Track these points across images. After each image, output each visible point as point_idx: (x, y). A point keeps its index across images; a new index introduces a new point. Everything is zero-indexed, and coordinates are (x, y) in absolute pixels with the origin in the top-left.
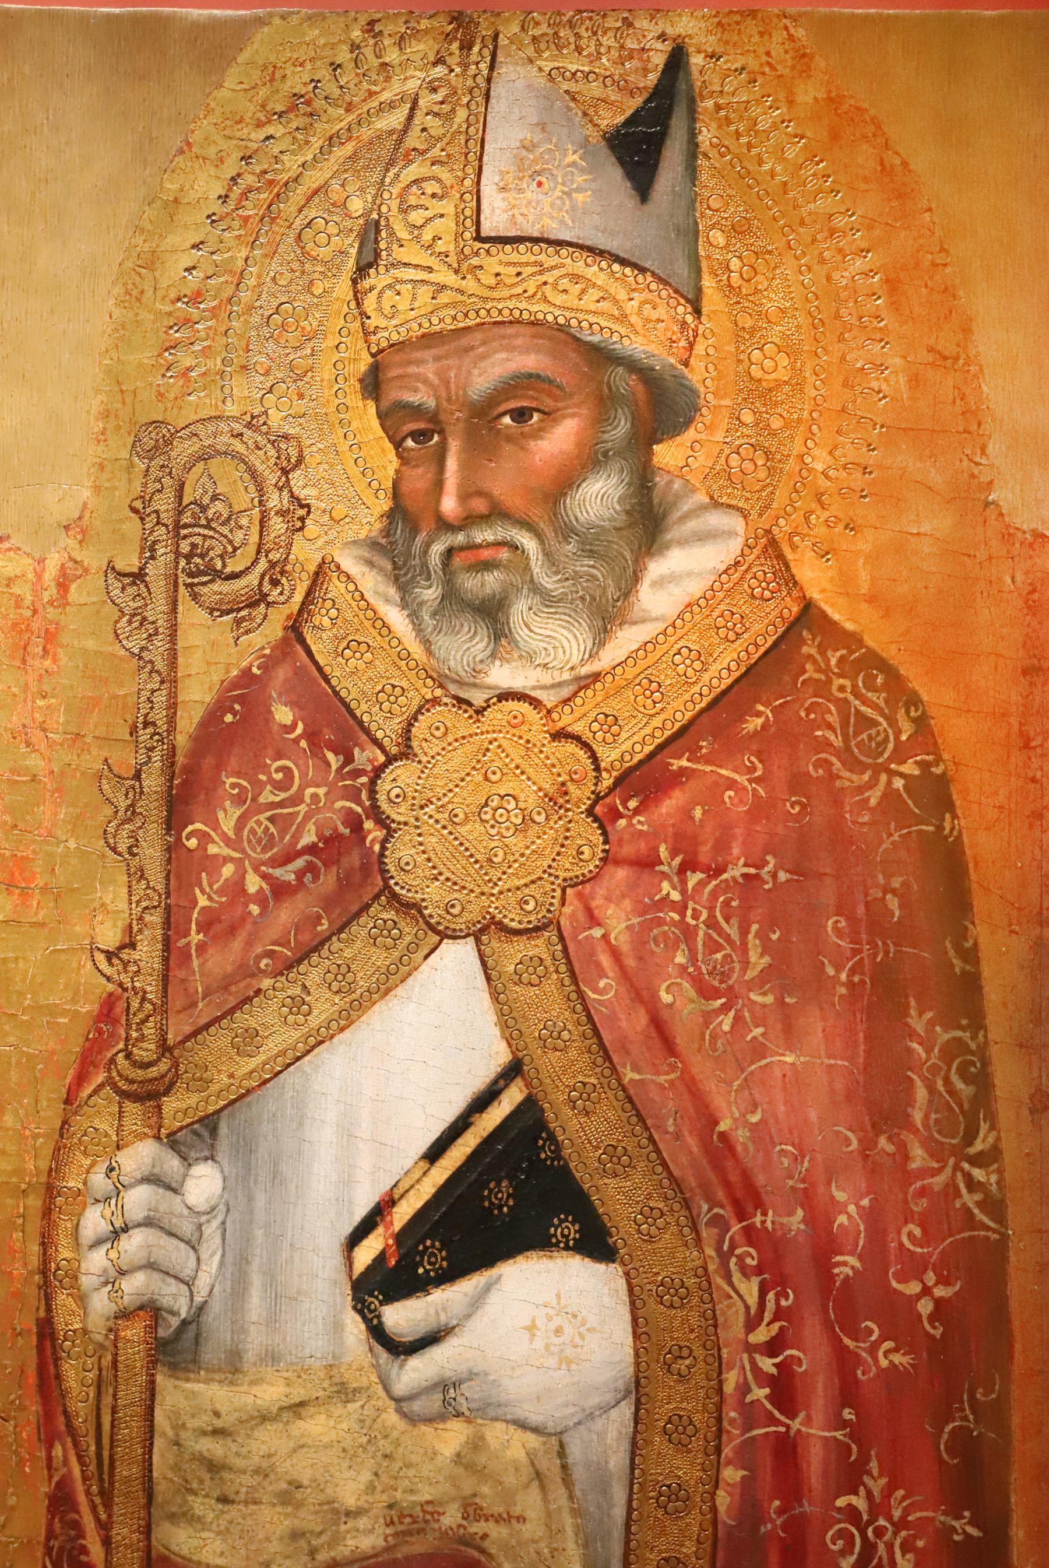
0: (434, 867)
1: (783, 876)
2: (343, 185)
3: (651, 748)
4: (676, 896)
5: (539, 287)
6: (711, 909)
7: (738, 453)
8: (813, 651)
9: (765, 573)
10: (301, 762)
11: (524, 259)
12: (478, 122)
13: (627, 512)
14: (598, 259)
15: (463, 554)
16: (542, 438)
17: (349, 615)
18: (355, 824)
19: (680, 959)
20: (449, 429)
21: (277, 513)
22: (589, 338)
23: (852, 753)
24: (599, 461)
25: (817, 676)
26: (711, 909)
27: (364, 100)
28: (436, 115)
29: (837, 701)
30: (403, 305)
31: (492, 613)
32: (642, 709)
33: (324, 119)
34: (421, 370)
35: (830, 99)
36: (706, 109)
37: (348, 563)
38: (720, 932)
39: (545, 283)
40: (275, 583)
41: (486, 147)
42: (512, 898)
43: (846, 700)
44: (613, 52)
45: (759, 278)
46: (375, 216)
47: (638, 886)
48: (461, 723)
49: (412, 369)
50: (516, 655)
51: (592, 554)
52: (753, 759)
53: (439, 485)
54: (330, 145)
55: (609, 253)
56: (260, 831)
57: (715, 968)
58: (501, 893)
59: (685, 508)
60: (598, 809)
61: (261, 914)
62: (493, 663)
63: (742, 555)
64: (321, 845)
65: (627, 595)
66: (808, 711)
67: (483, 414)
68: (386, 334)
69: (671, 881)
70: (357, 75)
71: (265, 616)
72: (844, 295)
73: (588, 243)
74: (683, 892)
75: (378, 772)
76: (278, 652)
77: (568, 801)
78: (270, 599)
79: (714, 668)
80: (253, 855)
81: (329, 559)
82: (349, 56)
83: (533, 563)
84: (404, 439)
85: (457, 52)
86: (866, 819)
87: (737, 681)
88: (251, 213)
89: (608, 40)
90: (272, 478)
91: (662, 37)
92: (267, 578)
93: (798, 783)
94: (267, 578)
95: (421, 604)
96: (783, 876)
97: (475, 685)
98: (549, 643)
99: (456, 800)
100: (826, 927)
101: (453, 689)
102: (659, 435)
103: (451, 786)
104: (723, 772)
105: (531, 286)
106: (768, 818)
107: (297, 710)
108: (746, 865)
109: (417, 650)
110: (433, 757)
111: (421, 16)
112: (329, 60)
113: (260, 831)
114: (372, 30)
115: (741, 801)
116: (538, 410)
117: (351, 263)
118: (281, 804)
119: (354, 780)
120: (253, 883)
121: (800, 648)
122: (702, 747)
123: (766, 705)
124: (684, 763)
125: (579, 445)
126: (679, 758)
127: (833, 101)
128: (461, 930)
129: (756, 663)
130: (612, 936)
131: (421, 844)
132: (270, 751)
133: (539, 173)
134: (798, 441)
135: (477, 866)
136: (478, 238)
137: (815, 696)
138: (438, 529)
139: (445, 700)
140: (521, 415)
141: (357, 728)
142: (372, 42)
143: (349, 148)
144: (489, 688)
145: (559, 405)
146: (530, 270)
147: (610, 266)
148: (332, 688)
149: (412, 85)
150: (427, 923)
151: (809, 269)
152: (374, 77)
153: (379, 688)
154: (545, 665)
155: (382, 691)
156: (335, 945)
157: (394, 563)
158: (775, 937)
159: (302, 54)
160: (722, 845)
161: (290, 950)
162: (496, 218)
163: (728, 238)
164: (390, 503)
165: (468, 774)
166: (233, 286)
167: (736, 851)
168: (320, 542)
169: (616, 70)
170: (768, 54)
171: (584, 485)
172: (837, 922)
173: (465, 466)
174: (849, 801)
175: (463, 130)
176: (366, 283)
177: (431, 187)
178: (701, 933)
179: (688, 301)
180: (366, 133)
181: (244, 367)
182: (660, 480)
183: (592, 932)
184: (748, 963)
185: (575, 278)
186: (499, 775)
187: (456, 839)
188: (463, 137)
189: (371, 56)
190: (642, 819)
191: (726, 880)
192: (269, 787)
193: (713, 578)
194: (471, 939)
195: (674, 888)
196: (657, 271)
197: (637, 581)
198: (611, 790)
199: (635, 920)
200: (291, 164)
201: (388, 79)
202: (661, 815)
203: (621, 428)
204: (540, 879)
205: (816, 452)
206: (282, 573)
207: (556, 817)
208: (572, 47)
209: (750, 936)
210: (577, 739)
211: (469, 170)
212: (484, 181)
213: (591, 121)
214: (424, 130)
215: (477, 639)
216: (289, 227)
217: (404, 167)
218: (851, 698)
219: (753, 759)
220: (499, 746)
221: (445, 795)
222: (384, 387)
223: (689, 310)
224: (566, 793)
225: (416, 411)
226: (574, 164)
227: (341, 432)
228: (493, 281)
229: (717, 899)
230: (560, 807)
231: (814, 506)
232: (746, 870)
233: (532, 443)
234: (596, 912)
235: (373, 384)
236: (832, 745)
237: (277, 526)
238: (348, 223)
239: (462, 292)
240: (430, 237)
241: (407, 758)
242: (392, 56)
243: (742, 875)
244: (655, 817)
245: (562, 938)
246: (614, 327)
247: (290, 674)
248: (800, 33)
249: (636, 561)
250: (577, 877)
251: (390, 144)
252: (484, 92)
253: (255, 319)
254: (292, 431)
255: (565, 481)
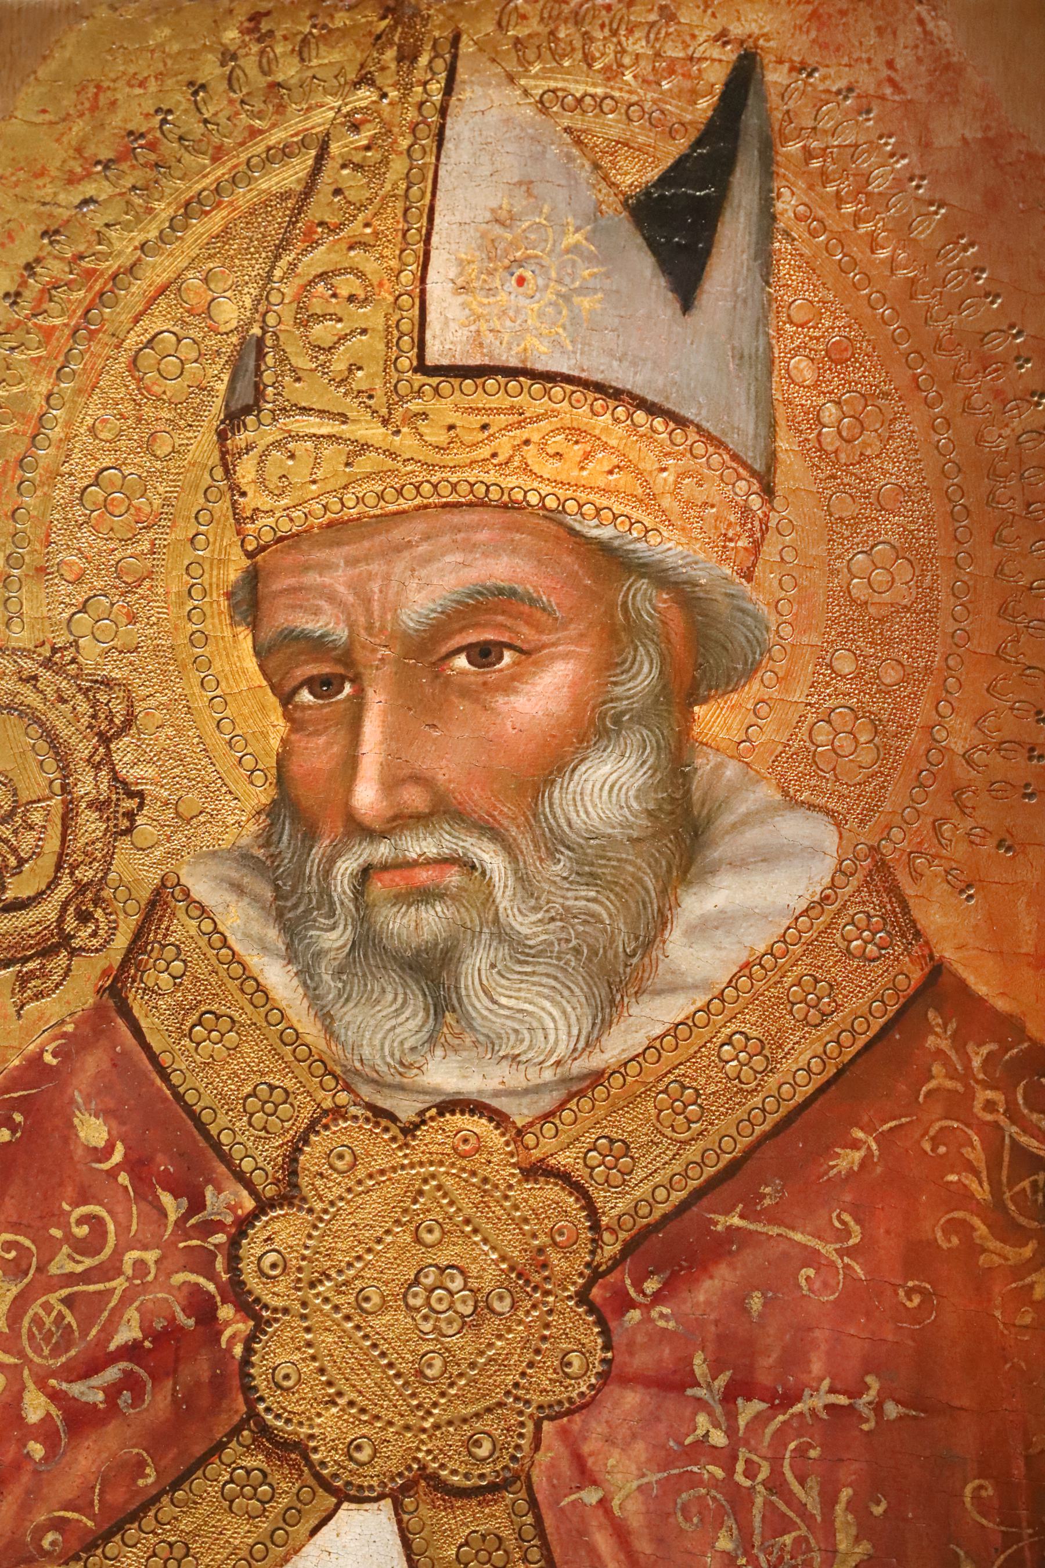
0: (330, 1384)
1: (892, 1410)
2: (206, 280)
3: (683, 1194)
4: (718, 1438)
5: (517, 448)
6: (776, 1462)
7: (829, 722)
8: (945, 1044)
9: (869, 917)
10: (119, 1209)
11: (494, 402)
12: (424, 179)
13: (650, 813)
14: (612, 403)
15: (387, 876)
16: (516, 691)
17: (202, 970)
18: (203, 1308)
19: (725, 1543)
20: (369, 674)
21: (89, 806)
22: (595, 533)
23: (1005, 1208)
24: (607, 731)
25: (949, 1084)
26: (776, 1462)
27: (242, 144)
28: (358, 167)
29: (981, 1127)
30: (300, 472)
31: (432, 971)
32: (668, 1132)
33: (179, 174)
34: (327, 580)
35: (988, 142)
36: (788, 156)
37: (201, 889)
38: (789, 1498)
39: (527, 442)
40: (84, 917)
41: (437, 221)
42: (454, 1436)
43: (996, 1125)
44: (643, 63)
45: (869, 436)
46: (256, 331)
47: (658, 1419)
48: (380, 1150)
49: (313, 578)
50: (468, 1041)
51: (592, 879)
52: (846, 1217)
53: (351, 763)
54: (187, 215)
55: (630, 394)
56: (48, 1321)
57: (781, 1559)
58: (437, 1427)
59: (743, 809)
60: (595, 1292)
61: (46, 1459)
62: (432, 1051)
63: (833, 886)
64: (147, 1344)
65: (648, 945)
66: (935, 1142)
67: (425, 648)
68: (271, 521)
69: (711, 1414)
70: (231, 102)
71: (69, 969)
72: (1003, 465)
73: (598, 377)
74: (731, 1432)
75: (244, 1225)
76: (87, 1030)
77: (547, 1279)
78: (76, 943)
79: (788, 1065)
80: (37, 1360)
81: (172, 880)
82: (218, 71)
83: (498, 893)
84: (296, 690)
85: (393, 66)
86: (1028, 1320)
87: (821, 1090)
88: (57, 322)
89: (637, 44)
90: (83, 748)
91: (722, 38)
92: (71, 909)
93: (918, 1257)
94: (71, 909)
95: (318, 955)
96: (892, 1410)
97: (402, 1088)
98: (522, 1021)
99: (367, 1274)
100: (962, 1495)
101: (367, 1092)
102: (703, 692)
103: (360, 1250)
104: (798, 1237)
105: (504, 445)
106: (868, 1315)
107: (114, 1124)
108: (832, 1390)
109: (310, 1029)
110: (332, 1203)
111: (335, 7)
112: (184, 78)
113: (48, 1321)
114: (256, 29)
115: (825, 1285)
116: (510, 647)
117: (217, 406)
118: (85, 1277)
119: (204, 1240)
120: (36, 1407)
121: (925, 1038)
122: (763, 1196)
123: (868, 1129)
124: (736, 1221)
125: (577, 703)
126: (727, 1212)
127: (993, 144)
128: (371, 1488)
129: (852, 1061)
130: (616, 1503)
131: (309, 1344)
132: (70, 1191)
133: (519, 263)
134: (925, 704)
135: (399, 1382)
136: (421, 367)
137: (946, 1118)
138: (349, 834)
139: (353, 1110)
140: (484, 654)
141: (211, 1153)
142: (255, 48)
143: (217, 220)
144: (425, 1092)
145: (545, 638)
146: (503, 419)
147: (630, 416)
148: (173, 1088)
149: (321, 119)
150: (317, 1476)
151: (948, 424)
152: (259, 106)
153: (248, 1089)
154: (515, 1057)
155: (253, 1094)
156: (167, 1510)
157: (277, 888)
158: (878, 1510)
159: (142, 67)
160: (794, 1357)
161: (92, 1517)
162: (450, 337)
163: (820, 371)
164: (273, 792)
165: (388, 1232)
166: (27, 440)
167: (817, 1367)
168: (158, 853)
169: (647, 110)
170: (890, 64)
171: (582, 768)
172: (981, 1487)
173: (393, 735)
174: (999, 1289)
175: (400, 192)
176: (241, 438)
177: (347, 285)
178: (759, 1501)
179: (754, 473)
180: (243, 197)
181: (41, 570)
182: (704, 763)
183: (583, 1494)
184: (835, 1552)
185: (575, 433)
186: (437, 1234)
187: (366, 1337)
188: (400, 205)
189: (253, 72)
190: (666, 1311)
191: (801, 1413)
192: (66, 1249)
193: (786, 923)
194: (387, 1504)
195: (717, 1425)
196: (706, 425)
197: (664, 924)
198: (617, 1262)
199: (653, 1477)
200: (123, 245)
201: (281, 109)
202: (697, 1304)
203: (642, 678)
204: (501, 1405)
205: (952, 721)
206: (97, 901)
207: (529, 1304)
208: (579, 55)
209: (839, 1509)
210: (564, 1177)
211: (409, 257)
212: (432, 275)
213: (605, 178)
214: (338, 192)
215: (407, 1014)
216: (118, 347)
217: (304, 252)
218: (1003, 1121)
219: (846, 1217)
220: (439, 1187)
221: (350, 1265)
222: (264, 606)
223: (756, 487)
224: (545, 1266)
225: (317, 646)
226: (575, 249)
227: (195, 677)
228: (442, 438)
229: (786, 1446)
230: (535, 1289)
231: (950, 809)
232: (833, 1399)
233: (501, 700)
234: (590, 1462)
235: (250, 600)
236: (972, 1196)
237: (91, 825)
238: (212, 342)
239: (392, 455)
240: (342, 366)
241: (291, 1205)
242: (288, 71)
243: (826, 1407)
244: (687, 1308)
245: (533, 1503)
246: (635, 515)
247: (106, 1065)
248: (942, 28)
249: (663, 892)
250: (560, 1403)
251: (281, 216)
252: (435, 130)
253: (60, 493)
254: (116, 674)
255: (552, 761)
